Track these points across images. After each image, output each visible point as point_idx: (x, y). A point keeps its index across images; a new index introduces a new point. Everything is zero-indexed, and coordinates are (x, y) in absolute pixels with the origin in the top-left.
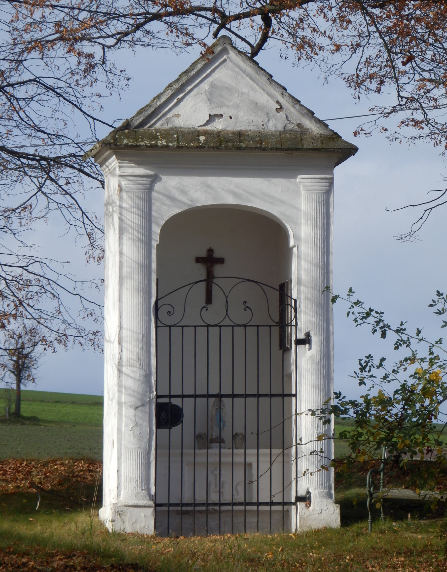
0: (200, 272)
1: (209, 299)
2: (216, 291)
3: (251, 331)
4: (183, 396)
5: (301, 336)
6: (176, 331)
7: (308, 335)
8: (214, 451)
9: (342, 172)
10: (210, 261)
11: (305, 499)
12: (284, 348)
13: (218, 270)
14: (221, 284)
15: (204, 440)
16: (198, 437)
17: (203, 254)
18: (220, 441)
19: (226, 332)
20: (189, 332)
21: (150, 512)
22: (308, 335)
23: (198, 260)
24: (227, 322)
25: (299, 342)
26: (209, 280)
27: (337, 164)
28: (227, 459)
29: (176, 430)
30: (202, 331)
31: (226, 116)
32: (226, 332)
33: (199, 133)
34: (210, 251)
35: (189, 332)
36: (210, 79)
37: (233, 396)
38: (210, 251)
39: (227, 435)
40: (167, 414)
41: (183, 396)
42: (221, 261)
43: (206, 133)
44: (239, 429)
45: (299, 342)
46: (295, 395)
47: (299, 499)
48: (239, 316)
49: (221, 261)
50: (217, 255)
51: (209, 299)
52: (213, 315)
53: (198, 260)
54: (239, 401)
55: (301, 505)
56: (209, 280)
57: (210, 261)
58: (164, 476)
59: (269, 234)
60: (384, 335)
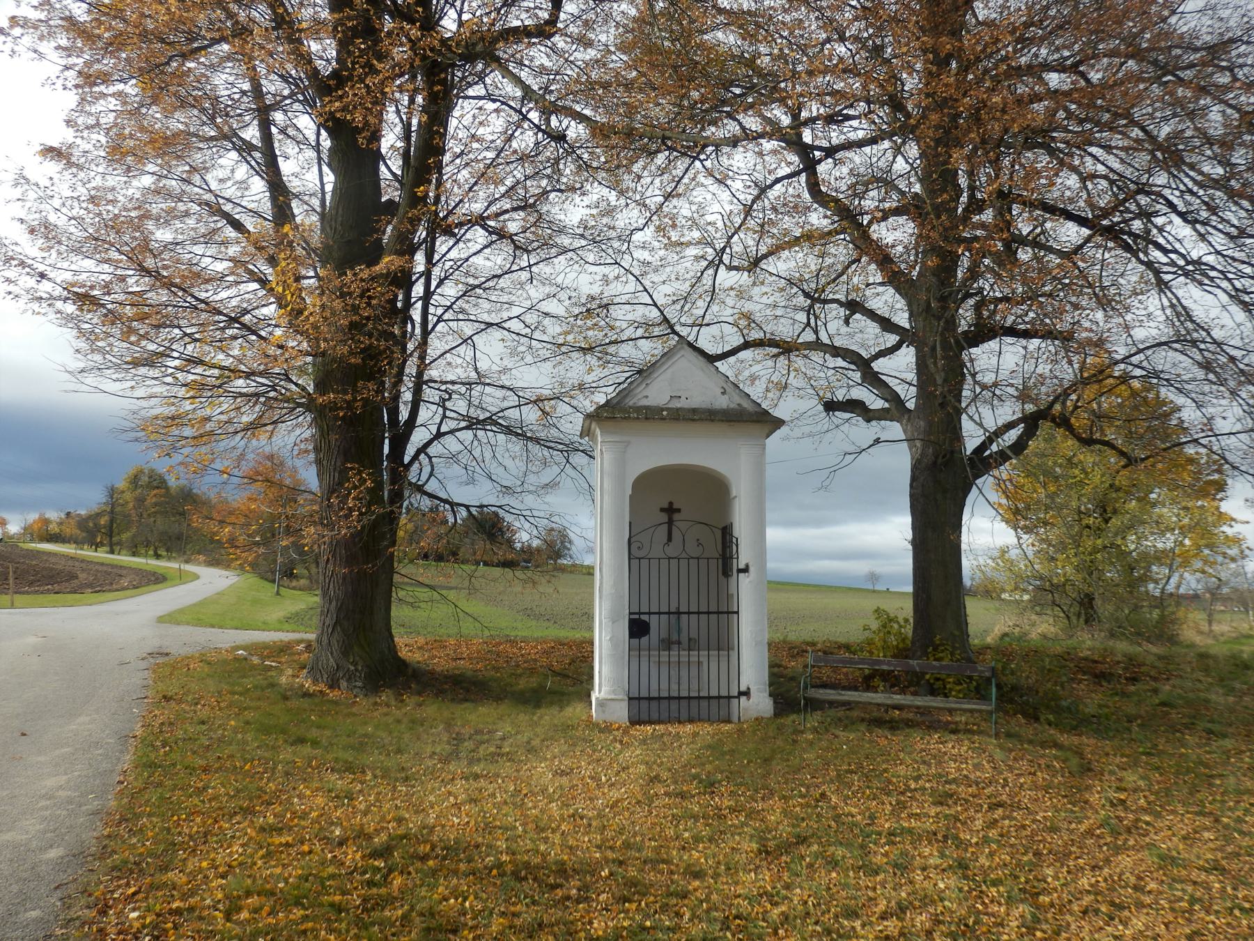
0: (664, 517)
1: (670, 539)
2: (675, 532)
3: (703, 563)
4: (650, 613)
5: (742, 566)
6: (644, 563)
7: (747, 566)
8: (674, 653)
9: (775, 441)
10: (670, 510)
11: (747, 693)
12: (726, 571)
13: (676, 516)
14: (680, 525)
15: (667, 644)
16: (661, 641)
17: (666, 506)
18: (679, 643)
19: (684, 563)
20: (654, 563)
21: (625, 704)
22: (747, 566)
23: (662, 510)
24: (684, 555)
25: (740, 571)
26: (670, 523)
27: (768, 436)
28: (684, 659)
29: (644, 640)
30: (664, 563)
31: (683, 398)
32: (684, 563)
33: (663, 410)
34: (671, 504)
35: (654, 563)
36: (670, 371)
37: (689, 613)
38: (671, 504)
39: (684, 639)
40: (638, 628)
41: (650, 613)
42: (679, 510)
43: (667, 409)
44: (694, 635)
45: (740, 571)
46: (737, 613)
47: (741, 694)
48: (693, 550)
49: (679, 510)
50: (675, 506)
51: (670, 539)
52: (672, 550)
53: (662, 510)
54: (694, 617)
55: (743, 699)
56: (670, 523)
57: (670, 510)
58: (634, 676)
59: (714, 489)
60: (51, 152)
